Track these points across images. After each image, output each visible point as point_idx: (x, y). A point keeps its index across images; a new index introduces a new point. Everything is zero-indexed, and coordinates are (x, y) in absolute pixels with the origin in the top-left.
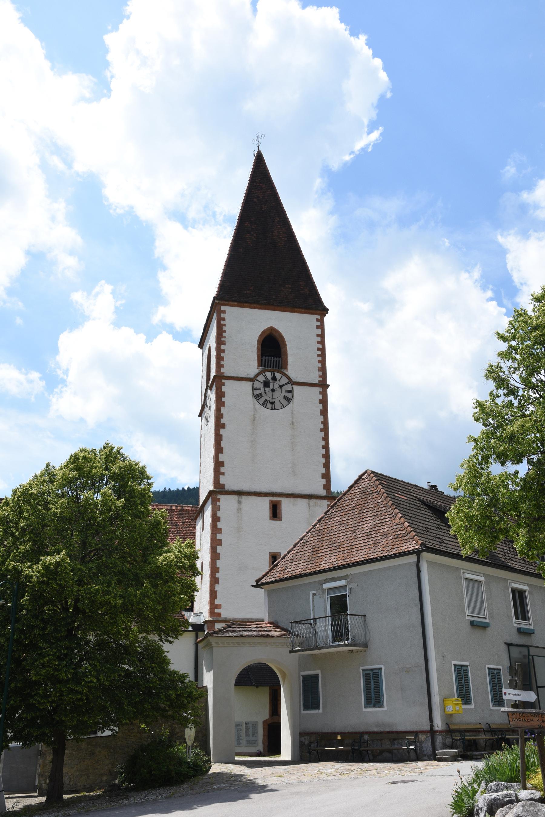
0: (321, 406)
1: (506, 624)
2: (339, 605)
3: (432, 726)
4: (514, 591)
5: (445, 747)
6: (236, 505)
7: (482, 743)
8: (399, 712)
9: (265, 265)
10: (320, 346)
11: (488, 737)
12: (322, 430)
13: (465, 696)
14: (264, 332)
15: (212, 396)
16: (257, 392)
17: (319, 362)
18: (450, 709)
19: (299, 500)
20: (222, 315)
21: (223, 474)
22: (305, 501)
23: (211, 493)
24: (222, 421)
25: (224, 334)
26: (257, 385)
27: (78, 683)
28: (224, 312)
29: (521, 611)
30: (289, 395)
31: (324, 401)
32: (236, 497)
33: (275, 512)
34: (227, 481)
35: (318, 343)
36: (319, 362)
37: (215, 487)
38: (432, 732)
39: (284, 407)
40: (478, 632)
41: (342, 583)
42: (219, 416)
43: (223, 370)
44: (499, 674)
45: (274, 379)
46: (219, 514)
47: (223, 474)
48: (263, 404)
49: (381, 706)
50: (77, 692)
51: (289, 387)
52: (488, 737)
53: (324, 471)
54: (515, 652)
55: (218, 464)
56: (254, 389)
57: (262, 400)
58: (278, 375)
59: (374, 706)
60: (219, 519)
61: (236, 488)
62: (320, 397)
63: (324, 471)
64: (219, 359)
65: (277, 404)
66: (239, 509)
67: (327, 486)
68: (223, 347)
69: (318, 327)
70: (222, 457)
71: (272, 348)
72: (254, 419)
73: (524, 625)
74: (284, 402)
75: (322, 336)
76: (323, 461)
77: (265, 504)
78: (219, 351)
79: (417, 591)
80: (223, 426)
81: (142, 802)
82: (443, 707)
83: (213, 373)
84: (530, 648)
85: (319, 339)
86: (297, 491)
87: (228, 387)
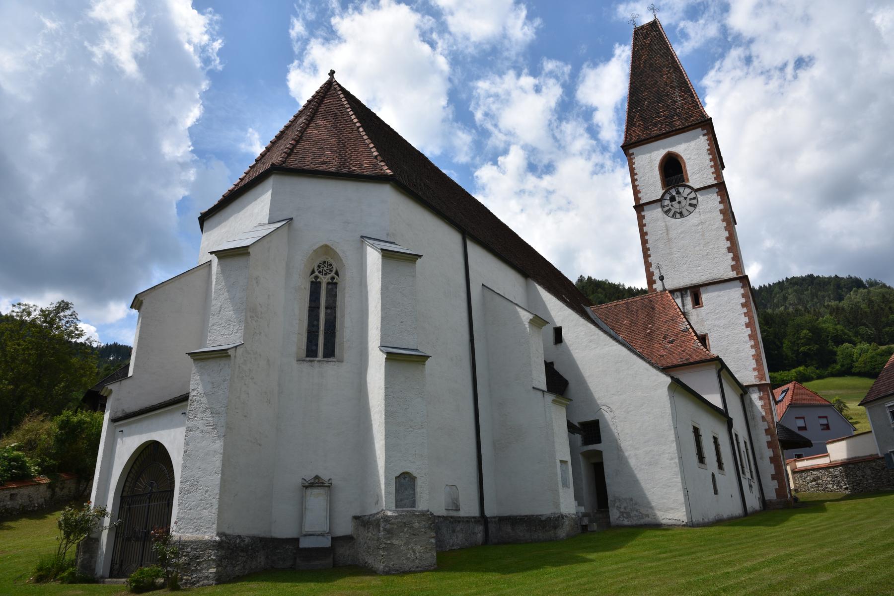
25: (713, 169)
26: (667, 202)
30: (694, 202)
39: (691, 213)
51: (693, 195)
58: (681, 190)
62: (640, 195)
65: (685, 213)
71: (672, 169)
74: (691, 209)
84: (724, 370)
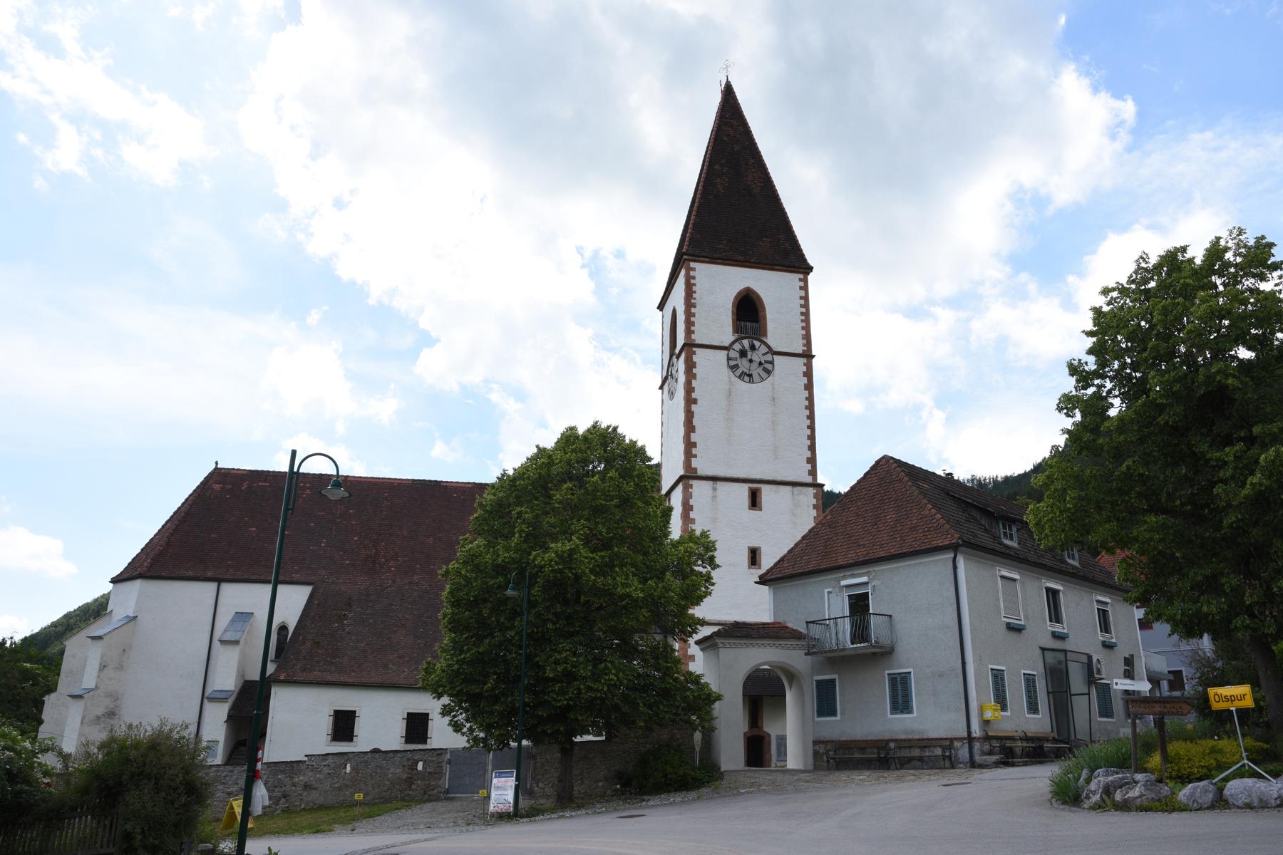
0: (805, 380)
1: (1041, 630)
2: (859, 604)
3: (969, 733)
4: (1048, 590)
5: (984, 753)
6: (710, 492)
7: (1018, 751)
8: (932, 718)
9: (736, 213)
10: (804, 310)
11: (1025, 744)
12: (806, 408)
13: (1001, 701)
14: (739, 293)
15: (681, 365)
16: (732, 363)
17: (803, 328)
18: (988, 715)
19: (782, 487)
20: (692, 273)
21: (695, 456)
22: (788, 488)
23: (681, 478)
24: (694, 395)
26: (733, 354)
27: (597, 681)
28: (694, 269)
29: (1056, 616)
30: (769, 367)
31: (809, 374)
32: (711, 483)
33: (754, 501)
34: (702, 465)
35: (802, 306)
36: (803, 328)
37: (686, 471)
38: (970, 739)
40: (1013, 635)
41: (865, 579)
42: (689, 389)
43: (693, 336)
44: (1034, 680)
45: (753, 348)
46: (692, 502)
47: (695, 456)
48: (739, 377)
49: (910, 712)
50: (597, 690)
52: (1025, 744)
53: (809, 454)
54: (1050, 657)
55: (690, 446)
56: (729, 359)
57: (739, 372)
58: (757, 343)
59: (902, 712)
60: (691, 508)
61: (710, 473)
63: (809, 454)
64: (689, 324)
65: (756, 377)
66: (714, 497)
67: (813, 472)
68: (693, 310)
69: (801, 288)
70: (694, 437)
71: (748, 310)
72: (730, 393)
73: (1058, 629)
74: (764, 374)
75: (806, 298)
76: (809, 443)
77: (744, 490)
78: (689, 314)
79: (953, 589)
80: (695, 401)
81: (923, 748)
82: (981, 710)
83: (681, 341)
85: (802, 302)
86: (779, 478)
87: (700, 356)
